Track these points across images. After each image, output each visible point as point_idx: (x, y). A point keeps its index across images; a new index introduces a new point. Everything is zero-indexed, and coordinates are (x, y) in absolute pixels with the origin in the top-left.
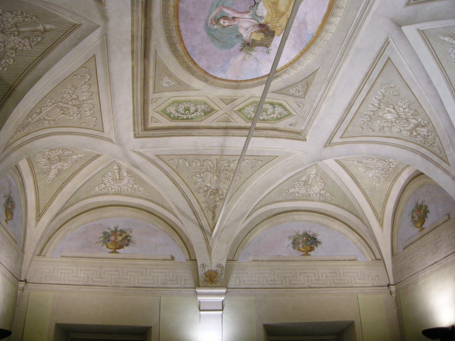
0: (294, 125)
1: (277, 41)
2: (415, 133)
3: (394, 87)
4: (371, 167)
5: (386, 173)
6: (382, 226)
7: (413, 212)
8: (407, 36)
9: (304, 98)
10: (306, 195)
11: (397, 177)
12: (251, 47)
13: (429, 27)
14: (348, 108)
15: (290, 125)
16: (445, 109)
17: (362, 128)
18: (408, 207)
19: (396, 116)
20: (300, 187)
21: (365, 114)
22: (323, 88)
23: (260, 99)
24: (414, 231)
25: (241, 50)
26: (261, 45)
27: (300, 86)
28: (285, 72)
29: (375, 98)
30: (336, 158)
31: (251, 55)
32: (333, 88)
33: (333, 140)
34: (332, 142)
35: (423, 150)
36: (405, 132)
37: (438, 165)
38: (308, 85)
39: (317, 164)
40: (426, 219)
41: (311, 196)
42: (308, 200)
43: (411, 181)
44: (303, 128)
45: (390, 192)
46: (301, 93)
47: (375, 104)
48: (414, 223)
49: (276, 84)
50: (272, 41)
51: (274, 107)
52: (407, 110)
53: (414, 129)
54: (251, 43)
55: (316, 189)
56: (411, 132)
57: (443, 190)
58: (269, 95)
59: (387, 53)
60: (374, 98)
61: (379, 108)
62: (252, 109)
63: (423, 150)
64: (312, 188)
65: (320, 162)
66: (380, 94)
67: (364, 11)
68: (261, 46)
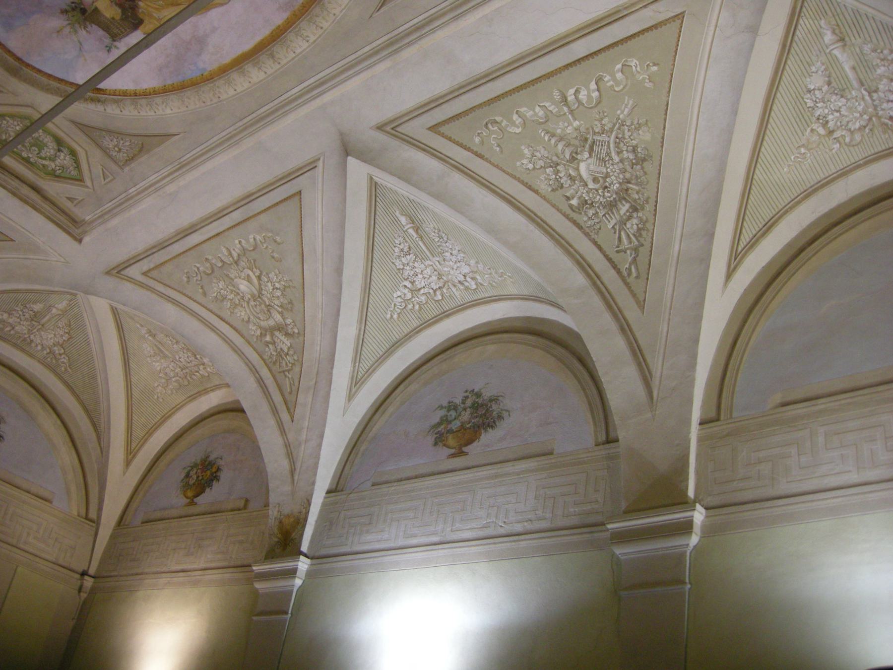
0: (76, 202)
1: (136, 37)
2: (268, 338)
3: (279, 244)
4: (167, 353)
5: (186, 377)
6: (128, 463)
7: (192, 467)
8: (348, 176)
9: (121, 168)
10: (25, 340)
11: (200, 394)
12: (85, 19)
13: (389, 185)
14: (187, 230)
15: (69, 198)
16: (337, 327)
17: (188, 278)
18: (190, 454)
19: (256, 292)
20: (22, 317)
21: (207, 259)
22: (164, 171)
23: (40, 116)
24: (178, 500)
25: (64, 12)
26: (106, 26)
27: (128, 144)
28: (116, 101)
29: (240, 242)
30: (115, 304)
31: (76, 32)
32: (182, 182)
33: (128, 269)
34: (125, 272)
35: (265, 372)
36: (254, 328)
37: (275, 411)
38: (142, 150)
39: (75, 295)
40: (208, 490)
41: (33, 345)
42: (23, 350)
43: (219, 412)
44: (87, 218)
45: (173, 413)
46: (121, 156)
47: (233, 252)
48: (184, 486)
49: (80, 109)
50: (128, 35)
51: (59, 150)
52: (279, 293)
53: (272, 330)
54: (89, 11)
55: (49, 337)
56: (263, 332)
57: (260, 455)
58: (58, 119)
59: (302, 182)
60: (237, 242)
61: (236, 263)
62: (18, 128)
63: (265, 372)
64: (43, 333)
65: (82, 294)
66: (252, 240)
67: (308, 92)
68: (103, 29)
